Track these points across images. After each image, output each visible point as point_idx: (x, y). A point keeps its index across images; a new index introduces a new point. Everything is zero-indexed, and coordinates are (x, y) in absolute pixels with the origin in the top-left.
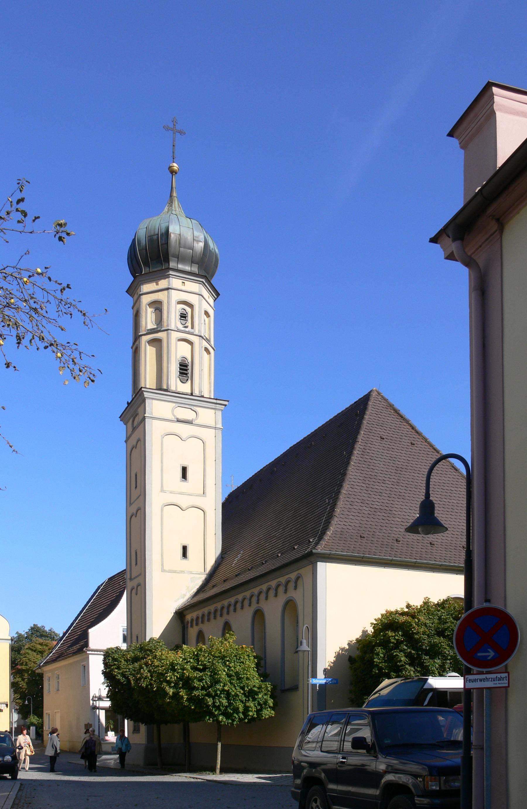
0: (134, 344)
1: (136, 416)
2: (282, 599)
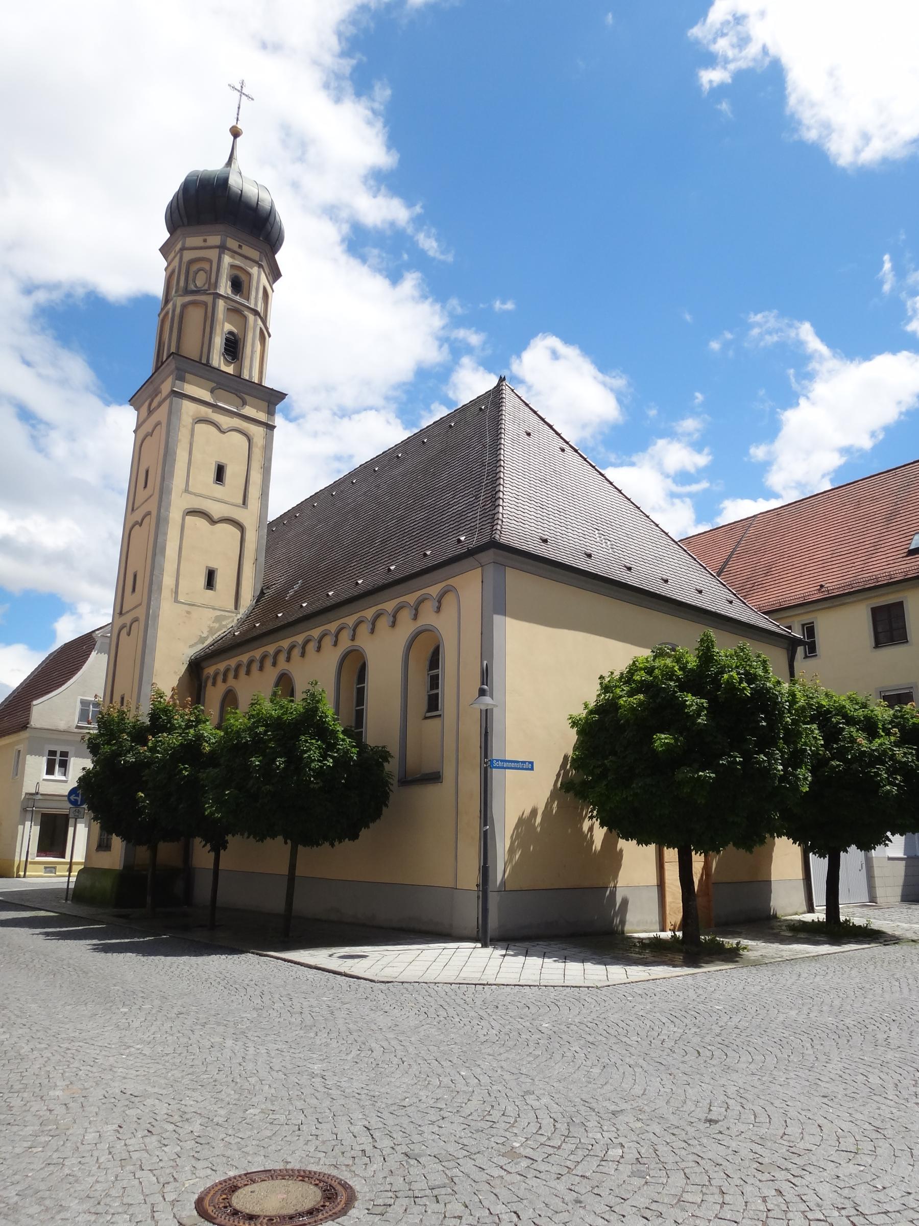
0: (162, 309)
2: (406, 628)
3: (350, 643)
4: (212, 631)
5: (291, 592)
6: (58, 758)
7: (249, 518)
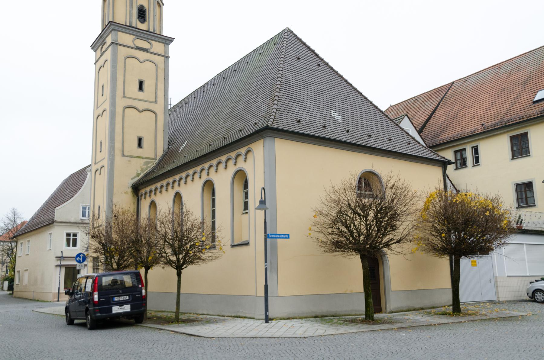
1: (104, 44)
2: (232, 169)
3: (207, 177)
4: (142, 170)
5: (182, 148)
6: (72, 237)
7: (159, 108)
